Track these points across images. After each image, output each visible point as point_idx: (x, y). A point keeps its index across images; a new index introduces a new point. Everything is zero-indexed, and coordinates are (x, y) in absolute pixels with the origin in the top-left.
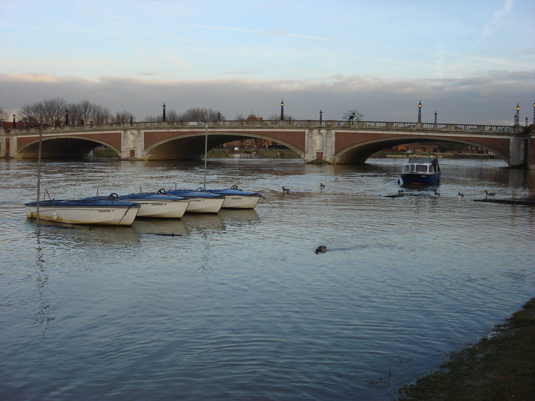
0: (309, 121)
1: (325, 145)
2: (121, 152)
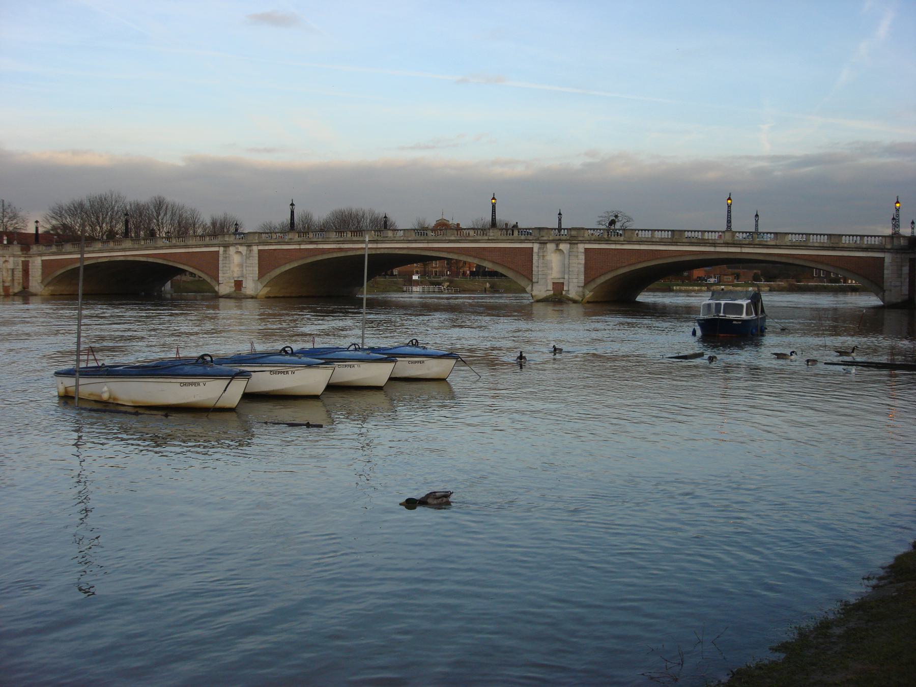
1: (567, 270)
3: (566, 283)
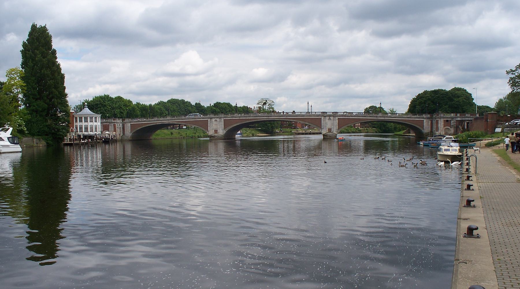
0: (323, 112)
2: (208, 131)
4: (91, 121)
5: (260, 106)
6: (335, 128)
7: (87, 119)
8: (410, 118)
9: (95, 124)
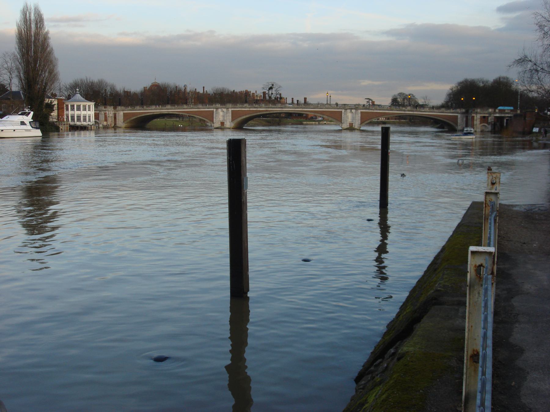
1: (354, 119)
3: (354, 123)
4: (85, 110)
5: (264, 91)
6: (357, 122)
7: (80, 107)
8: (443, 112)
9: (89, 113)
